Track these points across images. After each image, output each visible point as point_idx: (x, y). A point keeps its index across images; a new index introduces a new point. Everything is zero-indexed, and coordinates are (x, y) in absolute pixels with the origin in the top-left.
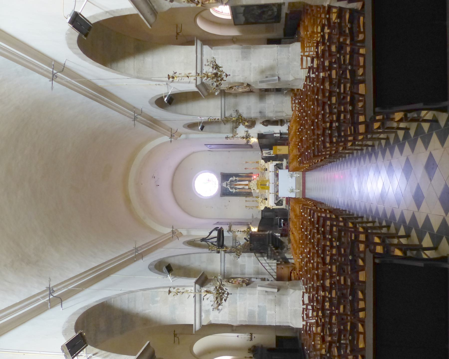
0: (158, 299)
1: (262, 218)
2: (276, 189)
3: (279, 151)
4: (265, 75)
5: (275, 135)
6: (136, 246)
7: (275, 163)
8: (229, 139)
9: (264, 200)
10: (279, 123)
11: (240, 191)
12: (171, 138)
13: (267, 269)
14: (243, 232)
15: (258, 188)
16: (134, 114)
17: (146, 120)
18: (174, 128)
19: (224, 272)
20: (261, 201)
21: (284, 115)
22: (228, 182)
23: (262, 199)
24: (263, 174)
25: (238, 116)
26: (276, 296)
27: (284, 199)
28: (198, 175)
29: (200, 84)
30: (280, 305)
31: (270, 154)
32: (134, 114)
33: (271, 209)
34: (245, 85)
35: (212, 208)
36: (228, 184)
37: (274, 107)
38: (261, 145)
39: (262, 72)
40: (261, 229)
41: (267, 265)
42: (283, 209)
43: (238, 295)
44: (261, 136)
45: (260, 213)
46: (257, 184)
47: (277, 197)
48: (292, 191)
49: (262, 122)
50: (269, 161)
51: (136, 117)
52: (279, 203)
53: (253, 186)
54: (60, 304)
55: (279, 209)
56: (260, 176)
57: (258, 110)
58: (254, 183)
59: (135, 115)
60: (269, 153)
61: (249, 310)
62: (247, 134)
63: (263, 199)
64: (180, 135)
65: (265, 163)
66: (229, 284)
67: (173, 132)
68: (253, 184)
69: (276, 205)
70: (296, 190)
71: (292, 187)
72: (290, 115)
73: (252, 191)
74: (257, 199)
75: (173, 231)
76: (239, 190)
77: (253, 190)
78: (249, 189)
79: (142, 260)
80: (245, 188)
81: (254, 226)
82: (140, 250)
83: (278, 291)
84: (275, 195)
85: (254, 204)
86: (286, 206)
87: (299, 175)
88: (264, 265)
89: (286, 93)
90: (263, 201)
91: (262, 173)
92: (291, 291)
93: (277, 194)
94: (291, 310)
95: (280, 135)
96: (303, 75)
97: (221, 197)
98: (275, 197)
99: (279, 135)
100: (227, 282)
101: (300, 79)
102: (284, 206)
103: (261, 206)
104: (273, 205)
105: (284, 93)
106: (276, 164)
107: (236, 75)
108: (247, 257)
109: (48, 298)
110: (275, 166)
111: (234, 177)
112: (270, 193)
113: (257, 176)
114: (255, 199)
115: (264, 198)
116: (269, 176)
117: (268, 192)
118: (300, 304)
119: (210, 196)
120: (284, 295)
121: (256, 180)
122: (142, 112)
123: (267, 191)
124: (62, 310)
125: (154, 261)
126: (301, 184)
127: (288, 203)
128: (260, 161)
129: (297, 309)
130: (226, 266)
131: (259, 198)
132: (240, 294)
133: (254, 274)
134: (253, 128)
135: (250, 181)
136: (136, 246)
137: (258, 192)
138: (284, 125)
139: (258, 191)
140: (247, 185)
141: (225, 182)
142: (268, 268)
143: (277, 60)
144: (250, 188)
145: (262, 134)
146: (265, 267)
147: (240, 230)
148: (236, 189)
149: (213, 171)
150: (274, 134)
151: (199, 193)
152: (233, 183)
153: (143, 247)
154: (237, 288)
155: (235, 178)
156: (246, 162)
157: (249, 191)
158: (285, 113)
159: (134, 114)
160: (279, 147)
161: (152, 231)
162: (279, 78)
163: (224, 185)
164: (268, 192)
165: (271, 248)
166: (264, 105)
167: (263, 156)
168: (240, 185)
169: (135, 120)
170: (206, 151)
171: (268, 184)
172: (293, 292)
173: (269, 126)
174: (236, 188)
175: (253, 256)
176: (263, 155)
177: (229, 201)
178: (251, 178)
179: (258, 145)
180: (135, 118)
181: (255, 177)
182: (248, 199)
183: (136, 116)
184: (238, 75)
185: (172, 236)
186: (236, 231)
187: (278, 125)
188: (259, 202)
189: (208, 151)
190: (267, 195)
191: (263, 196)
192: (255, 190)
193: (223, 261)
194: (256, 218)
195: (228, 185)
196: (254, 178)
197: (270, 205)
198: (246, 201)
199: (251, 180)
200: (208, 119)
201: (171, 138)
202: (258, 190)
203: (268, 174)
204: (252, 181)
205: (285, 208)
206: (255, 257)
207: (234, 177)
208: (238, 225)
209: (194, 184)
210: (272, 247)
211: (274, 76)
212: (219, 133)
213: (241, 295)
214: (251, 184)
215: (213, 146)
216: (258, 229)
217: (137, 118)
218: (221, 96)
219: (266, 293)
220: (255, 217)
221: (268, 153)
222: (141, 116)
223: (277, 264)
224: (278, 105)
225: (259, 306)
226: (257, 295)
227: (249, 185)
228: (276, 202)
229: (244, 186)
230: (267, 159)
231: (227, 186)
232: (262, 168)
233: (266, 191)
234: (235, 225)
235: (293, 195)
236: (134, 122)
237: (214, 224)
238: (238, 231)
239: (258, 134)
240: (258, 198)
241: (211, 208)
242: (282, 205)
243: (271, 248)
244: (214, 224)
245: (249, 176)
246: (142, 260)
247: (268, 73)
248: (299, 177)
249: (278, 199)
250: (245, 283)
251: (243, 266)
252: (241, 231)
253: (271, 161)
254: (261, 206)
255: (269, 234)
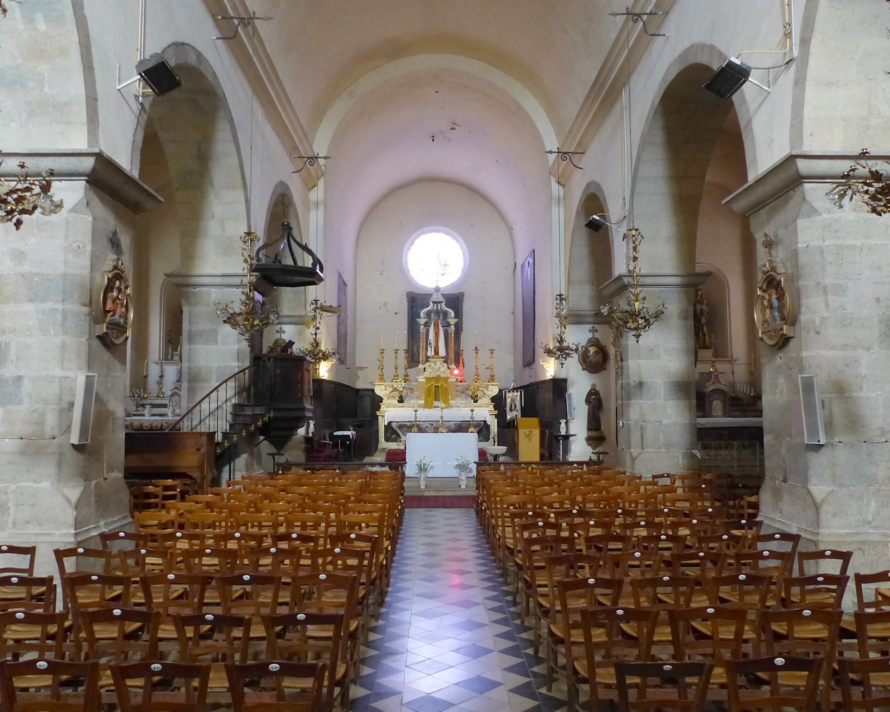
0: (42, 26)
1: (358, 391)
2: (426, 424)
3: (525, 433)
4: (830, 398)
5: (563, 422)
6: (259, 18)
7: (493, 424)
8: (557, 304)
9: (398, 395)
10: (594, 434)
11: (421, 335)
12: (559, 152)
13: (202, 404)
14: (313, 341)
15: (428, 379)
16: (647, 14)
17: (631, 44)
18: (585, 161)
19: (195, 286)
20: (396, 389)
21: (634, 451)
22: (444, 306)
23: (401, 390)
24: (463, 392)
25: (647, 318)
26: (54, 438)
27: (402, 444)
28: (457, 241)
29: (797, 171)
30: (22, 453)
31: (511, 410)
32: (647, 14)
33: (378, 413)
34: (786, 330)
35: (381, 274)
36: (437, 307)
37: (655, 421)
38: (536, 386)
39: (841, 389)
40: (326, 388)
41: (214, 406)
42: (377, 441)
43: (60, 306)
44: (559, 386)
45: (369, 387)
46: (438, 378)
47: (408, 427)
48: (422, 468)
49: (597, 389)
50: (495, 408)
51: (639, 19)
52: (392, 432)
53: (433, 368)
54: (223, 37)
55: (377, 431)
56: (457, 386)
57: (646, 378)
58: (440, 371)
59: (644, 14)
60: (513, 407)
61: (7, 344)
62: (572, 350)
63: (402, 392)
64: (563, 184)
65: (492, 396)
66: (103, 278)
67: (575, 159)
68: (440, 368)
69: (386, 424)
70: (424, 479)
71: (432, 467)
72: (633, 468)
73: (421, 366)
74: (401, 377)
75: (317, 158)
76: (425, 332)
77: (425, 368)
78: (427, 359)
79: (217, 38)
80: (429, 348)
81: (332, 370)
82: (247, 34)
83: (73, 445)
84: (411, 422)
85: (389, 370)
86: (384, 449)
87: (463, 487)
88: (214, 395)
89: (693, 456)
90: (396, 393)
91: (467, 390)
92: (74, 493)
93: (415, 429)
94: (6, 493)
95: (563, 436)
96: (833, 531)
97: (407, 295)
98: (405, 422)
99: (563, 432)
100: (116, 271)
101: (817, 523)
102: (383, 444)
103: (383, 387)
104: (386, 417)
105: (693, 451)
106: (489, 424)
107: (831, 298)
108: (238, 350)
109: (232, 14)
110: (483, 421)
111: (456, 320)
112: (416, 411)
113: (459, 378)
114: (401, 372)
115: (404, 394)
116: (458, 407)
117: (420, 406)
118: (28, 522)
119: (410, 269)
120: (59, 465)
121: (449, 375)
122: (654, 35)
123: (422, 402)
124: (213, 40)
125: (214, 73)
126: (441, 494)
127: (389, 461)
128: (495, 384)
129: (10, 513)
130: (213, 290)
131: (403, 383)
132: (64, 313)
133: (190, 368)
134: (580, 367)
135: (446, 360)
136: (259, 18)
137: (419, 380)
138: (589, 444)
139: (421, 379)
140: (437, 352)
141: (443, 298)
142: (205, 405)
143: (884, 440)
144: (429, 361)
145: (565, 389)
146: (207, 399)
147: (318, 331)
148: (427, 325)
149: (467, 274)
150: (565, 421)
151: (416, 242)
152: (441, 317)
153: (255, 40)
154: (88, 302)
155: (454, 323)
156: (492, 351)
157: (422, 357)
158: (640, 454)
159: (648, 11)
160: (536, 433)
161: (319, 111)
162: (819, 447)
163: (437, 297)
164: (420, 406)
165: (263, 416)
166: (662, 393)
167: (505, 392)
168: (437, 335)
169: (631, 14)
170: (515, 259)
171: (441, 404)
172: (68, 500)
173: (587, 407)
174: (428, 325)
175: (240, 364)
176: (509, 392)
177: (396, 313)
178: (453, 362)
179: (533, 380)
180: (634, 14)
181: (456, 372)
182: (402, 356)
183: (641, 18)
184: (827, 305)
185: (304, 156)
186: (318, 323)
187: (589, 429)
188: (393, 383)
189: (515, 264)
190: (412, 401)
191: (409, 392)
192: (422, 375)
193: (226, 281)
194: (357, 376)
195: (436, 305)
196: (454, 369)
197: (386, 409)
198: (396, 351)
199: (449, 362)
200: (637, 230)
201: (559, 152)
202: (424, 380)
203: (464, 404)
204: (445, 364)
205: (380, 446)
206: (237, 369)
207: (456, 320)
208: (338, 332)
209: (436, 231)
210: (266, 419)
211: (826, 432)
212: (569, 281)
213: (59, 317)
214: (438, 363)
215: (529, 271)
216: (324, 380)
217: (636, 21)
218: (688, 275)
219: (65, 405)
220: (360, 373)
221: (513, 403)
222: (641, 30)
223: (211, 435)
224: (662, 435)
225: (19, 378)
226: (58, 372)
227: (436, 357)
228: (394, 425)
229: (433, 345)
230: (498, 402)
231: (434, 303)
232: (478, 389)
233: (421, 400)
234: (339, 324)
235: (410, 470)
236: (625, 12)
237: (340, 275)
238: (318, 328)
239: (565, 381)
240: (404, 379)
241: (381, 271)
242: (387, 439)
243: (263, 416)
244: (340, 275)
245: (456, 357)
246: (217, 38)
247: (837, 410)
248: (460, 486)
249: (400, 430)
250: (106, 333)
251: (211, 337)
252: (316, 334)
253: (496, 412)
254: (383, 387)
255: (304, 409)
